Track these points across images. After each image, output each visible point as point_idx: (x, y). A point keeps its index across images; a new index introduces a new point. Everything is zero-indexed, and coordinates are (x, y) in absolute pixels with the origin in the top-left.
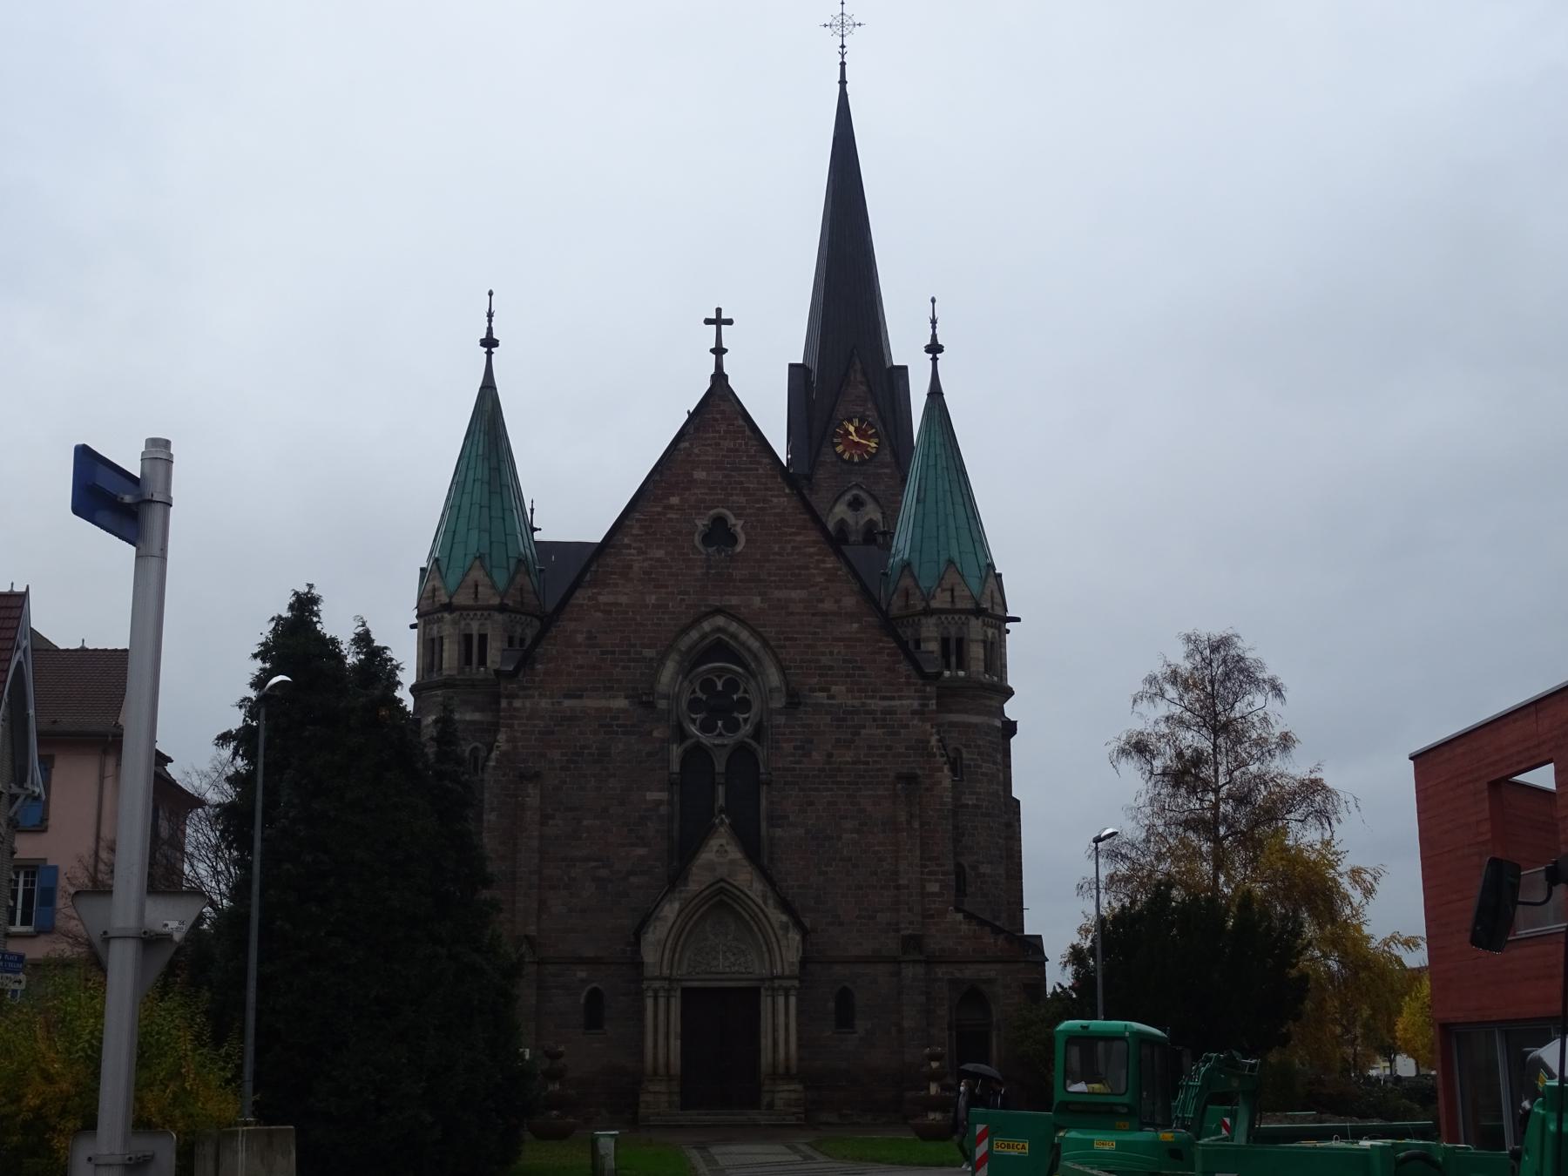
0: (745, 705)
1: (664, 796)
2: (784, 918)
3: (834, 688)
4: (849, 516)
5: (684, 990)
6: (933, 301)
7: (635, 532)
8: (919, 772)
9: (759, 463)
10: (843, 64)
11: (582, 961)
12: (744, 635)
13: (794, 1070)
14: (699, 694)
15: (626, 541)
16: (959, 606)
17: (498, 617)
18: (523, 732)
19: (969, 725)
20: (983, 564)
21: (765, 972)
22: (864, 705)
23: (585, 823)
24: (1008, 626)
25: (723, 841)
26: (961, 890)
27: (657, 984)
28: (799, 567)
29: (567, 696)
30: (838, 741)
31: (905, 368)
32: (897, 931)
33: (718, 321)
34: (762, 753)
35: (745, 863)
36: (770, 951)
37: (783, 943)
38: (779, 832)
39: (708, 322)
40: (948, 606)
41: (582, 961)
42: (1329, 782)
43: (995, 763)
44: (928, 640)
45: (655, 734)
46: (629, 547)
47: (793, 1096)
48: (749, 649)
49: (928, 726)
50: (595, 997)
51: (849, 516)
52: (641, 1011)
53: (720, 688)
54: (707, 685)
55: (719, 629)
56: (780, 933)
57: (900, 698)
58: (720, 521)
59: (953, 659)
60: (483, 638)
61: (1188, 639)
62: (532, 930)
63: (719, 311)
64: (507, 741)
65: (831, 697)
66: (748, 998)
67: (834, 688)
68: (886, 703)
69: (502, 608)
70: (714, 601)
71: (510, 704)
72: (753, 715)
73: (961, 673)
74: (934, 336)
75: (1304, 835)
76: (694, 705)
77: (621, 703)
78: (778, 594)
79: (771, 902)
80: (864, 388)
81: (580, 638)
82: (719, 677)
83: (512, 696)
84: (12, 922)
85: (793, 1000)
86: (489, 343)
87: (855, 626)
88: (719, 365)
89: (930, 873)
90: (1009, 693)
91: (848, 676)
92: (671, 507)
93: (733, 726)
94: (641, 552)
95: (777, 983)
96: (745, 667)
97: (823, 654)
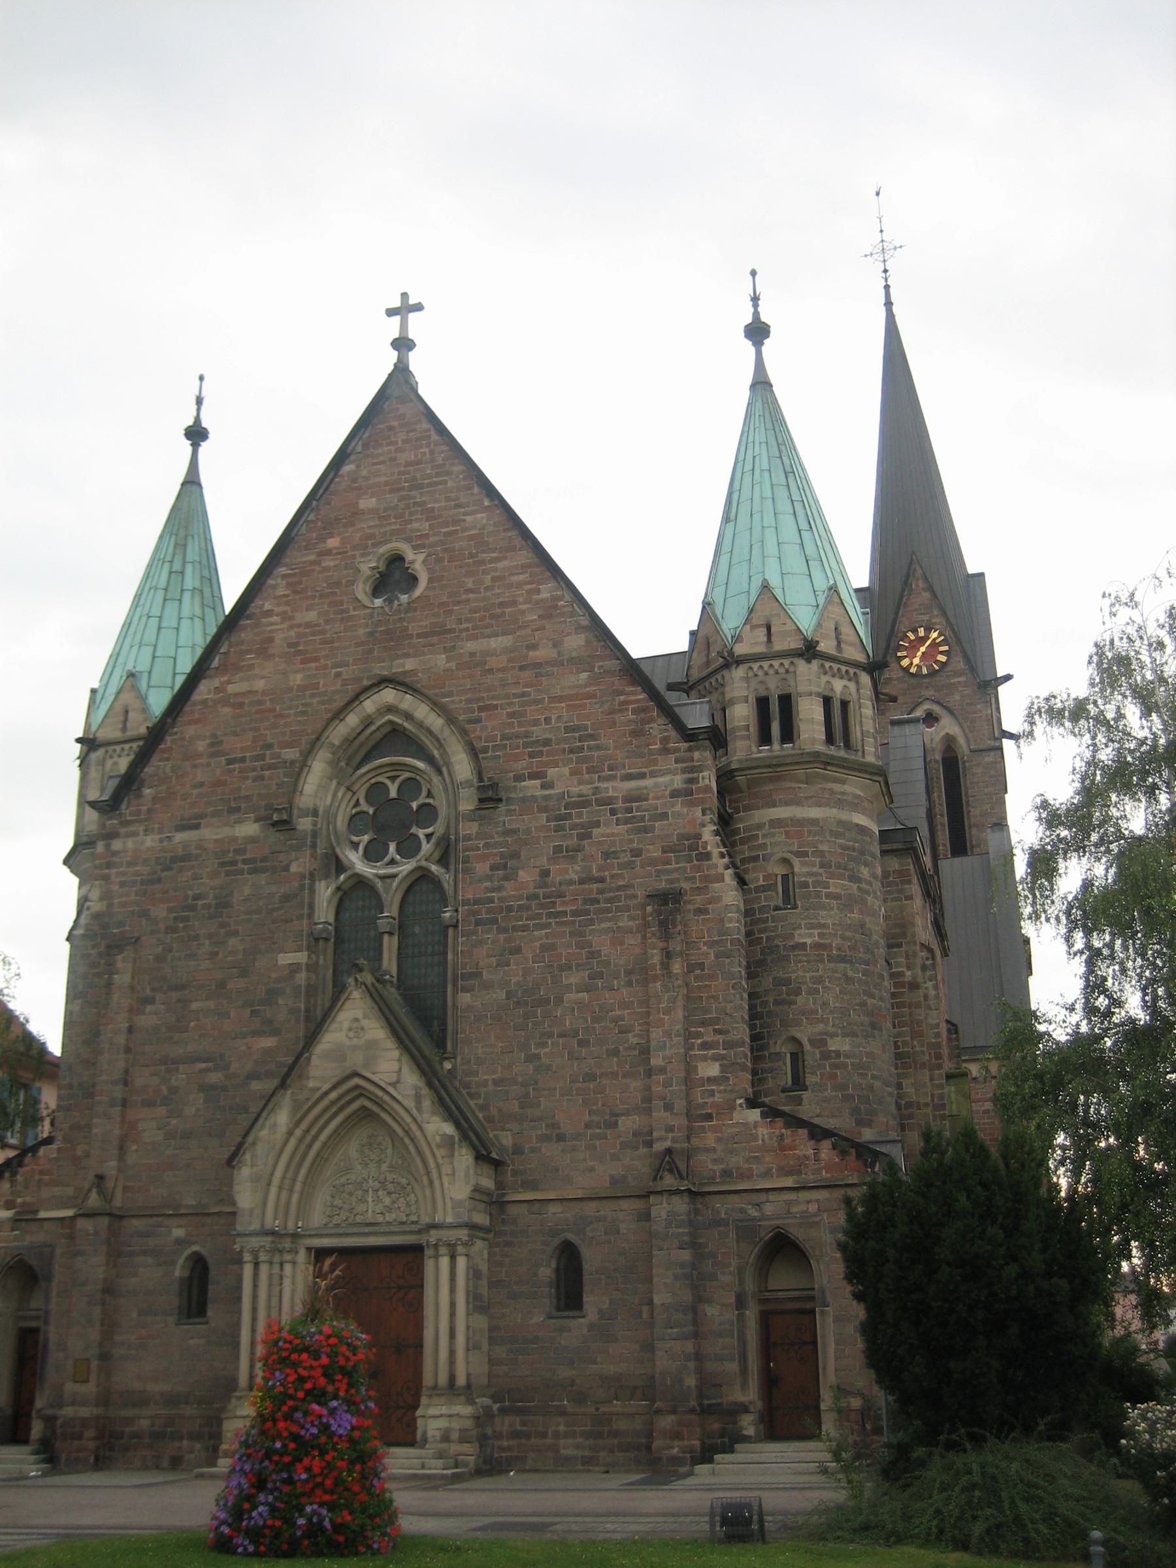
0: (428, 813)
1: (302, 957)
2: (449, 1129)
3: (551, 772)
7: (281, 592)
8: (685, 885)
9: (448, 473)
10: (887, 287)
12: (422, 711)
13: (461, 1381)
14: (364, 806)
15: (267, 606)
16: (779, 646)
18: (122, 884)
19: (801, 822)
20: (821, 584)
22: (597, 790)
23: (195, 1006)
25: (359, 1013)
27: (255, 1242)
28: (501, 604)
31: (982, 575)
32: (649, 1144)
33: (405, 309)
34: (446, 879)
35: (390, 1044)
36: (431, 1183)
37: (447, 1169)
39: (391, 312)
40: (761, 649)
45: (294, 868)
46: (269, 613)
48: (430, 732)
49: (698, 811)
53: (393, 794)
55: (390, 709)
56: (439, 1153)
57: (653, 774)
58: (397, 559)
59: (775, 728)
63: (405, 296)
64: (101, 899)
67: (551, 772)
68: (633, 784)
70: (380, 669)
71: (108, 846)
72: (438, 828)
74: (756, 314)
76: (356, 821)
77: (249, 829)
78: (470, 646)
79: (427, 1104)
80: (927, 595)
81: (201, 746)
82: (393, 779)
86: (196, 434)
87: (584, 676)
89: (705, 1046)
91: (571, 751)
92: (328, 552)
93: (409, 848)
94: (285, 617)
97: (536, 723)
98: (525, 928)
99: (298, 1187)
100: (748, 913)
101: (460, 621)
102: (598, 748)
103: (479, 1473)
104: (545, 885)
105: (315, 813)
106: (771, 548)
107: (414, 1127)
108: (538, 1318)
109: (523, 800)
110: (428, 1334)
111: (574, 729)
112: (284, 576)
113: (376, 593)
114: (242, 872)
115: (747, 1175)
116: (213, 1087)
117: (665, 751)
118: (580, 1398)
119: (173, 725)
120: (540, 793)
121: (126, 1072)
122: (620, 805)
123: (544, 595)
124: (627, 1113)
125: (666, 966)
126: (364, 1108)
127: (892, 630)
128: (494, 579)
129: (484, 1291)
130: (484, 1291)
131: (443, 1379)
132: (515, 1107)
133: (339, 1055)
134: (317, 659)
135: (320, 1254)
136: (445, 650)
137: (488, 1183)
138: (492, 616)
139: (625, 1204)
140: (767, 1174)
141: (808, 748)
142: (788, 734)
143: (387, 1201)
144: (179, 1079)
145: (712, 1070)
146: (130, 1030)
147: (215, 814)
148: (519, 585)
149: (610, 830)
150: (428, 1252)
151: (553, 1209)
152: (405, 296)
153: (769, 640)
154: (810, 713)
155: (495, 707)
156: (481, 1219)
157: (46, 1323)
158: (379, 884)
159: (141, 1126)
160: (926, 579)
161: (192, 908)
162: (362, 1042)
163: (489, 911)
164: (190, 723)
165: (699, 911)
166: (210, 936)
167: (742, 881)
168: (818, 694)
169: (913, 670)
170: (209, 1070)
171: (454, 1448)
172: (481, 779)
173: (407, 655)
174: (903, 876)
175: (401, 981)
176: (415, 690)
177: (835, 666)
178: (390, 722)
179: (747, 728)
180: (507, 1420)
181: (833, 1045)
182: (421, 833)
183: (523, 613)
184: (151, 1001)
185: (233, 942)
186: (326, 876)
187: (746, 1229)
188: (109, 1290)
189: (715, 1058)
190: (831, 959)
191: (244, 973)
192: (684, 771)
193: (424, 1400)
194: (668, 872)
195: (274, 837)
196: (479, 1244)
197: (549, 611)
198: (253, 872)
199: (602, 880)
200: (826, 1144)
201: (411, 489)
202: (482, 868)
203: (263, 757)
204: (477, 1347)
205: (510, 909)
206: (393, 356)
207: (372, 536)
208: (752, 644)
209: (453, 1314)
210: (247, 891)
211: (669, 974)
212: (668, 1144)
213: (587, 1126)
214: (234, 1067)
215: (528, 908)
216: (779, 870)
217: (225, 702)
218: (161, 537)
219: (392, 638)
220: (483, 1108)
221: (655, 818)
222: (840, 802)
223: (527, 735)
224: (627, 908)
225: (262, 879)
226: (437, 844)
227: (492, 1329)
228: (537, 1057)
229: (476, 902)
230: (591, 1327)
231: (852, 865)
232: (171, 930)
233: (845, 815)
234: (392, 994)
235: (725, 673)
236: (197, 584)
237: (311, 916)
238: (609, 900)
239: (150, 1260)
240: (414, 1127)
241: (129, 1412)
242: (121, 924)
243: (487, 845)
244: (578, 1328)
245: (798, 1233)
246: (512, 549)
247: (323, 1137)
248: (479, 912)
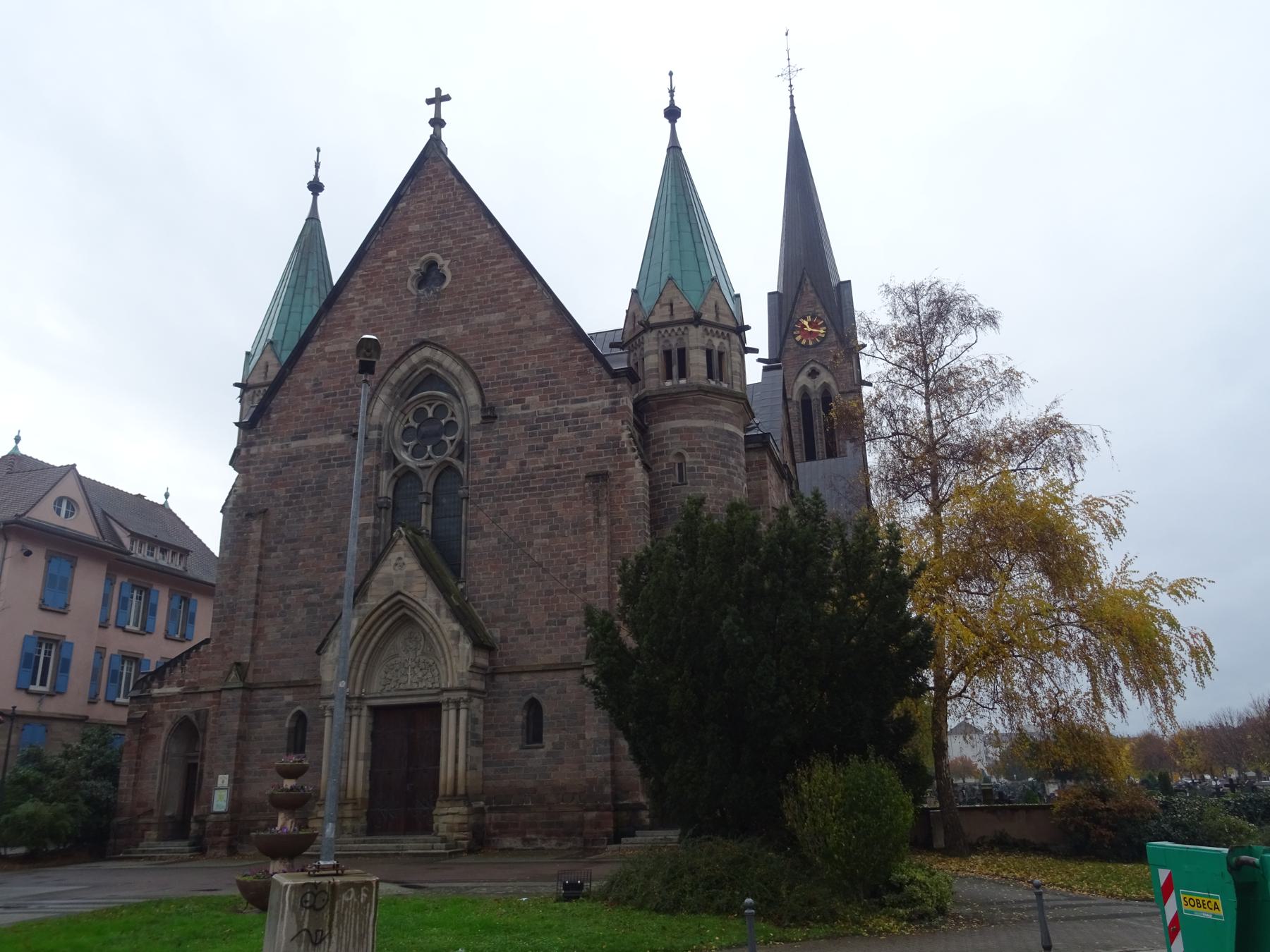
0: (452, 425)
2: (456, 627)
3: (528, 398)
4: (809, 383)
5: (371, 708)
6: (671, 74)
7: (358, 286)
8: (610, 470)
9: (465, 207)
10: (792, 97)
11: (289, 685)
12: (448, 361)
13: (461, 791)
15: (351, 295)
16: (678, 317)
18: (257, 475)
19: (689, 430)
23: (302, 552)
25: (401, 554)
28: (498, 292)
29: (295, 438)
30: (531, 448)
31: (849, 282)
33: (438, 99)
34: (461, 467)
35: (421, 573)
37: (454, 652)
39: (429, 102)
40: (667, 319)
41: (289, 685)
42: (1068, 418)
44: (649, 353)
46: (352, 300)
47: (458, 820)
49: (619, 423)
51: (809, 383)
53: (430, 415)
54: (420, 413)
57: (591, 399)
58: (432, 265)
59: (675, 369)
61: (888, 290)
62: (245, 658)
66: (432, 711)
68: (578, 406)
70: (422, 335)
71: (248, 451)
73: (683, 381)
75: (1035, 482)
78: (479, 319)
79: (443, 611)
80: (813, 295)
81: (308, 386)
84: (34, 683)
86: (316, 187)
87: (549, 337)
91: (541, 385)
92: (388, 260)
93: (439, 447)
94: (362, 303)
97: (518, 368)
98: (510, 499)
99: (362, 666)
100: (652, 488)
101: (471, 303)
102: (557, 383)
103: (470, 851)
104: (522, 471)
105: (380, 427)
107: (435, 626)
108: (514, 749)
109: (510, 417)
110: (443, 759)
111: (543, 371)
112: (361, 276)
113: (420, 286)
114: (333, 466)
116: (313, 604)
119: (290, 373)
120: (520, 412)
121: (257, 595)
122: (570, 419)
124: (572, 615)
125: (596, 521)
126: (405, 615)
127: (791, 318)
128: (494, 276)
129: (480, 732)
130: (480, 732)
131: (449, 791)
133: (388, 580)
135: (375, 710)
136: (462, 322)
137: (483, 661)
138: (492, 300)
141: (694, 381)
142: (683, 374)
146: (260, 569)
147: (317, 429)
148: (509, 279)
149: (565, 435)
150: (444, 707)
151: (525, 678)
152: (438, 90)
153: (672, 314)
154: (697, 360)
155: (493, 358)
156: (478, 684)
157: (202, 759)
158: (421, 473)
159: (266, 630)
162: (404, 572)
163: (488, 488)
164: (301, 371)
165: (619, 486)
166: (312, 507)
167: (647, 467)
168: (702, 348)
170: (309, 593)
172: (483, 404)
173: (438, 326)
174: (763, 465)
175: (434, 536)
176: (443, 348)
177: (715, 330)
178: (428, 369)
179: (657, 370)
180: (493, 815)
182: (447, 439)
183: (511, 297)
184: (274, 550)
185: (327, 511)
186: (388, 468)
188: (242, 737)
192: (611, 397)
193: (438, 804)
194: (599, 461)
196: (476, 702)
197: (528, 295)
198: (340, 466)
199: (558, 467)
201: (442, 218)
202: (483, 461)
203: (347, 393)
204: (474, 768)
205: (501, 487)
206: (431, 130)
207: (417, 249)
209: (457, 747)
210: (336, 478)
211: (600, 527)
213: (547, 624)
215: (512, 486)
216: (677, 461)
220: (483, 613)
221: (593, 427)
222: (716, 416)
223: (513, 375)
224: (574, 485)
226: (457, 447)
227: (485, 756)
228: (517, 580)
229: (481, 482)
230: (548, 754)
231: (723, 456)
232: (287, 504)
233: (719, 425)
234: (425, 542)
235: (645, 336)
236: (316, 284)
237: (376, 493)
238: (564, 480)
239: (269, 716)
240: (435, 626)
242: (256, 501)
243: (487, 446)
244: (538, 756)
246: (504, 256)
247: (379, 634)
248: (481, 489)
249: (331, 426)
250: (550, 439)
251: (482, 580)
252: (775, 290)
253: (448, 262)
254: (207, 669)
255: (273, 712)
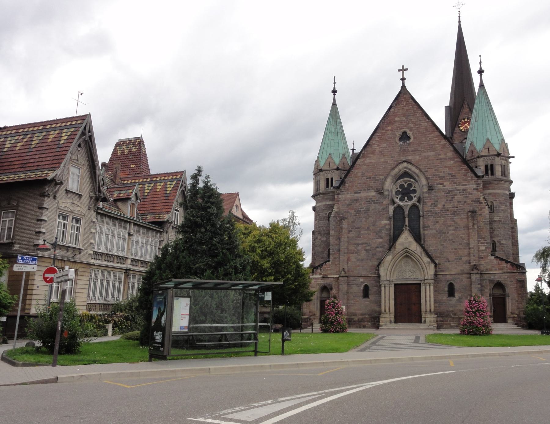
0: (414, 191)
1: (388, 222)
3: (445, 184)
5: (395, 285)
8: (476, 209)
10: (459, 17)
12: (413, 169)
13: (432, 310)
14: (399, 189)
15: (374, 143)
16: (491, 153)
17: (337, 172)
19: (495, 194)
20: (500, 138)
21: (422, 278)
23: (362, 232)
24: (510, 160)
25: (407, 235)
26: (494, 249)
27: (385, 283)
28: (432, 145)
29: (356, 193)
30: (447, 200)
32: (470, 263)
33: (403, 70)
34: (420, 206)
37: (428, 268)
38: (426, 232)
39: (399, 70)
40: (487, 154)
43: (506, 206)
46: (374, 144)
48: (415, 173)
50: (366, 288)
52: (380, 291)
55: (405, 168)
56: (427, 265)
57: (469, 185)
58: (405, 133)
59: (490, 172)
60: (332, 179)
63: (403, 66)
65: (445, 186)
67: (445, 184)
69: (338, 169)
70: (403, 158)
74: (481, 68)
76: (397, 193)
77: (373, 194)
78: (425, 154)
80: (468, 109)
81: (359, 174)
83: (338, 194)
85: (432, 287)
88: (403, 84)
89: (481, 243)
90: (511, 182)
93: (410, 199)
94: (378, 145)
95: (426, 281)
96: (414, 179)
97: (441, 172)
106: (488, 130)
108: (445, 298)
109: (439, 189)
111: (450, 174)
115: (491, 270)
117: (472, 180)
118: (455, 314)
123: (442, 143)
124: (464, 257)
125: (473, 226)
132: (439, 255)
133: (402, 244)
134: (387, 156)
139: (464, 275)
140: (496, 270)
142: (492, 174)
143: (411, 274)
144: (360, 248)
145: (483, 248)
148: (436, 140)
149: (459, 197)
152: (403, 66)
160: (468, 105)
161: (360, 211)
165: (480, 215)
166: (364, 217)
169: (463, 130)
171: (432, 324)
181: (502, 242)
182: (413, 195)
184: (352, 231)
185: (370, 219)
187: (491, 281)
189: (484, 246)
190: (502, 224)
191: (374, 225)
195: (379, 195)
198: (374, 203)
200: (509, 264)
202: (429, 204)
207: (398, 127)
208: (485, 153)
212: (474, 263)
214: (372, 246)
217: (365, 164)
218: (329, 119)
219: (405, 151)
221: (469, 194)
225: (377, 205)
230: (457, 300)
241: (353, 317)
242: (342, 214)
244: (453, 301)
245: (503, 282)
246: (434, 132)
249: (370, 189)
250: (454, 198)
251: (431, 244)
252: (448, 105)
253: (411, 133)
254: (330, 270)
255: (356, 284)
